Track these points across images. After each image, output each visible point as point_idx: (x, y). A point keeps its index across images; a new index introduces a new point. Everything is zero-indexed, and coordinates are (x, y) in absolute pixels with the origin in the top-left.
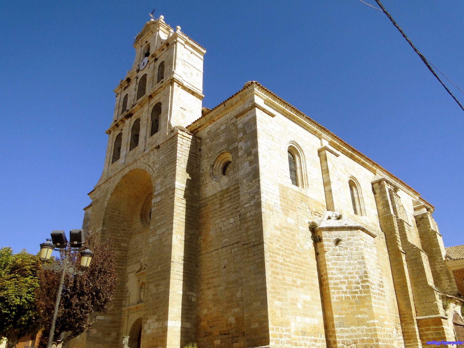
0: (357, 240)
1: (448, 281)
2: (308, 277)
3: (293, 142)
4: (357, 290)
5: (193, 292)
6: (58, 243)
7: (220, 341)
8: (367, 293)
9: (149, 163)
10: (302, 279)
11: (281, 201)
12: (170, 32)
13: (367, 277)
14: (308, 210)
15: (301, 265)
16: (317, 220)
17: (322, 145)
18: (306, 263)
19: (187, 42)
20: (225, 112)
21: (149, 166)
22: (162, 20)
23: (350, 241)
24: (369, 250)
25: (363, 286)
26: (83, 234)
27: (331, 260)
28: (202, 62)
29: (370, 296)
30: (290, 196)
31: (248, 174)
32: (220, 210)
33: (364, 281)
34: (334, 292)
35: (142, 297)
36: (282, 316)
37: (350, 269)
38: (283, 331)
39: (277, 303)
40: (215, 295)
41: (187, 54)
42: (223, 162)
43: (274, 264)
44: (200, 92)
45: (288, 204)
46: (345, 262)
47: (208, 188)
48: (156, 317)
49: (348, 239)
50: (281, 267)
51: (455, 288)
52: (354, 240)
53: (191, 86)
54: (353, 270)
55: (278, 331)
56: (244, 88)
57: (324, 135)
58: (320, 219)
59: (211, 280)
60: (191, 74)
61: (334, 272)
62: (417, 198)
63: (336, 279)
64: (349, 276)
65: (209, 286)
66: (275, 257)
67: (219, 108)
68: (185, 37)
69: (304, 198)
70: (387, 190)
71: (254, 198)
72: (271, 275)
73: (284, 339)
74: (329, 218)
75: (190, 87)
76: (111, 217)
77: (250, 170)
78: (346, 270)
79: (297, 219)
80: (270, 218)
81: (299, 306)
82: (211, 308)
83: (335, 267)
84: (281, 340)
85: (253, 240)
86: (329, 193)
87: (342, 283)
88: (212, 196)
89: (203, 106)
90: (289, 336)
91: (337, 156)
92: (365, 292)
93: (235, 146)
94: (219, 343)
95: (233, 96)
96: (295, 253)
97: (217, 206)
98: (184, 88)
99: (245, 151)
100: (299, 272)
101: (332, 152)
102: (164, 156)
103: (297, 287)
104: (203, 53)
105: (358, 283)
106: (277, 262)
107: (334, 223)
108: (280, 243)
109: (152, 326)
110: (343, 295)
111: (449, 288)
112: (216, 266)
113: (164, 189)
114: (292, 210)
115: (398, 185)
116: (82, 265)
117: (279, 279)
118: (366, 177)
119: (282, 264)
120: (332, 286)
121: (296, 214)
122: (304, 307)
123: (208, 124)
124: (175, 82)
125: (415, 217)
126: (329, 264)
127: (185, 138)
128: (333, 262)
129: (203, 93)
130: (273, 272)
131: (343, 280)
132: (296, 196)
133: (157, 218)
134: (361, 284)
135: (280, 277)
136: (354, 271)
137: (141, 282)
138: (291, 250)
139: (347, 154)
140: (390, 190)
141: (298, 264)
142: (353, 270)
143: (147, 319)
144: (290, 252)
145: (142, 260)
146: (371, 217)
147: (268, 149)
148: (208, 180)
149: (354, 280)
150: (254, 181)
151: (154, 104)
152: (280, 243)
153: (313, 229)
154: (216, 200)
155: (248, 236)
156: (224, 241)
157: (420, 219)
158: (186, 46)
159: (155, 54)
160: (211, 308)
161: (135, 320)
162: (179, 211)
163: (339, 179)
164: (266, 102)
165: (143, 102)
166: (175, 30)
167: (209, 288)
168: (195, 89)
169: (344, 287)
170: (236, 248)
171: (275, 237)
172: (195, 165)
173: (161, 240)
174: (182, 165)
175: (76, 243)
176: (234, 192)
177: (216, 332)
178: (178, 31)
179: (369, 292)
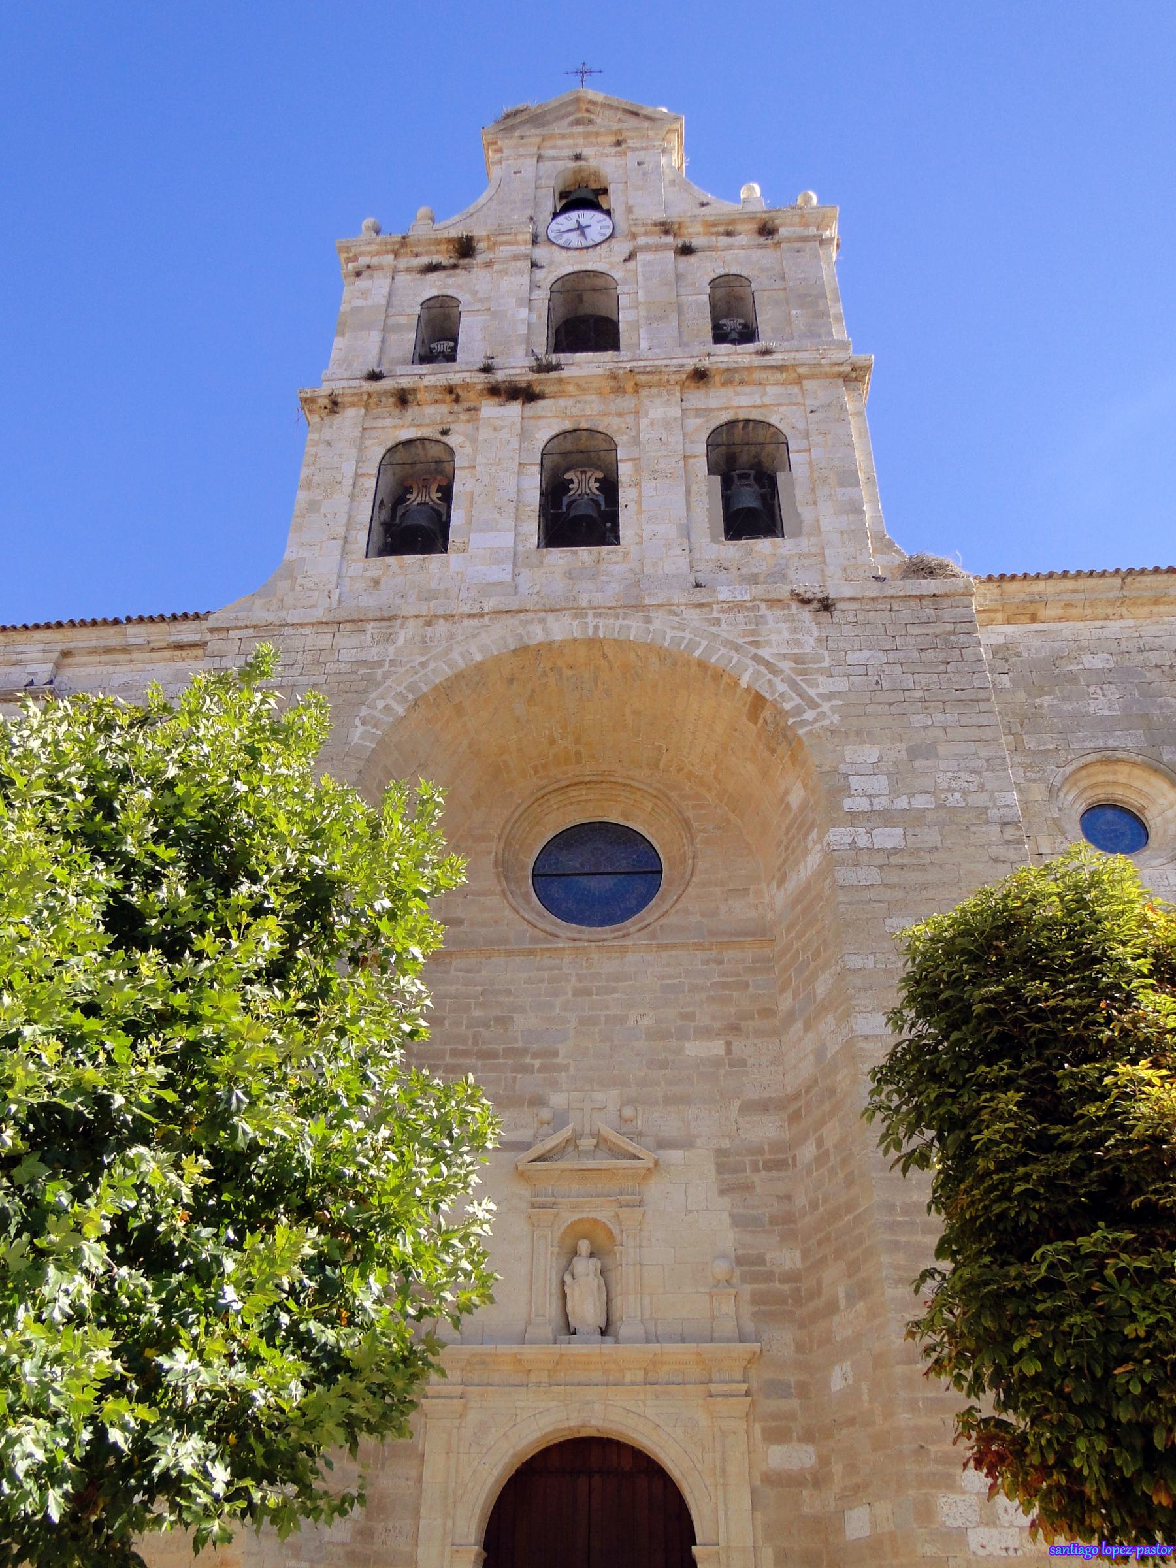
20: (1109, 611)
42: (1110, 790)
151: (725, 417)
159: (680, 225)
165: (643, 378)
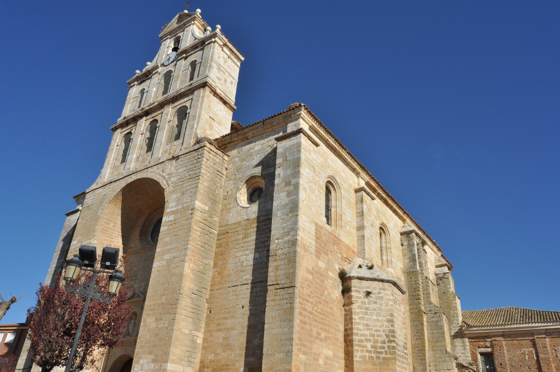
0: (387, 295)
1: (462, 348)
2: (332, 330)
3: (331, 177)
4: (383, 350)
8: (392, 355)
9: (164, 174)
10: (326, 332)
11: (316, 241)
13: (394, 337)
14: (339, 255)
15: (327, 316)
16: (346, 267)
17: (359, 184)
18: (332, 314)
21: (163, 177)
22: (198, 14)
23: (380, 295)
24: (397, 307)
25: (389, 347)
26: (121, 254)
27: (358, 313)
28: (238, 70)
29: (395, 359)
30: (324, 237)
31: (285, 206)
33: (390, 341)
34: (358, 350)
37: (377, 326)
39: (302, 357)
40: (226, 339)
41: (224, 58)
42: (252, 186)
43: (303, 312)
46: (373, 317)
47: (231, 214)
48: (152, 357)
49: (379, 293)
50: (309, 317)
51: (469, 357)
52: (385, 295)
53: (223, 95)
54: (380, 327)
56: (290, 110)
57: (363, 174)
58: (349, 266)
61: (361, 327)
62: (440, 254)
63: (361, 335)
64: (376, 333)
65: (219, 327)
68: (225, 39)
69: (337, 241)
70: (415, 243)
71: (289, 234)
74: (360, 267)
75: (223, 95)
78: (373, 326)
80: (304, 259)
81: (321, 361)
82: (219, 354)
83: (362, 322)
85: (282, 282)
86: (361, 238)
87: (367, 340)
88: (235, 224)
89: (233, 119)
91: (373, 199)
92: (390, 354)
95: (275, 116)
96: (322, 302)
97: (241, 237)
98: (215, 94)
100: (324, 324)
101: (368, 194)
103: (321, 340)
104: (240, 60)
105: (384, 343)
106: (305, 310)
107: (364, 272)
108: (311, 289)
110: (367, 354)
111: (462, 355)
112: (231, 305)
113: (180, 207)
114: (325, 253)
115: (426, 239)
116: (110, 291)
117: (306, 330)
118: (396, 224)
119: (311, 313)
120: (357, 343)
121: (327, 257)
122: (325, 363)
123: (240, 141)
125: (436, 275)
126: (356, 318)
127: (212, 152)
128: (360, 316)
129: (235, 104)
130: (301, 321)
131: (368, 338)
132: (329, 237)
134: (387, 344)
135: (307, 327)
136: (381, 329)
138: (319, 298)
139: (381, 198)
140: (418, 244)
141: (324, 315)
142: (380, 327)
143: (140, 358)
145: (135, 286)
146: (396, 269)
148: (232, 205)
149: (380, 339)
150: (290, 215)
153: (343, 277)
154: (239, 229)
156: (245, 277)
157: (441, 279)
158: (225, 49)
160: (219, 354)
163: (372, 225)
166: (214, 29)
167: (219, 330)
168: (227, 98)
169: (369, 345)
172: (219, 185)
173: (169, 266)
174: (205, 183)
175: (108, 263)
176: (263, 224)
178: (218, 31)
179: (394, 353)
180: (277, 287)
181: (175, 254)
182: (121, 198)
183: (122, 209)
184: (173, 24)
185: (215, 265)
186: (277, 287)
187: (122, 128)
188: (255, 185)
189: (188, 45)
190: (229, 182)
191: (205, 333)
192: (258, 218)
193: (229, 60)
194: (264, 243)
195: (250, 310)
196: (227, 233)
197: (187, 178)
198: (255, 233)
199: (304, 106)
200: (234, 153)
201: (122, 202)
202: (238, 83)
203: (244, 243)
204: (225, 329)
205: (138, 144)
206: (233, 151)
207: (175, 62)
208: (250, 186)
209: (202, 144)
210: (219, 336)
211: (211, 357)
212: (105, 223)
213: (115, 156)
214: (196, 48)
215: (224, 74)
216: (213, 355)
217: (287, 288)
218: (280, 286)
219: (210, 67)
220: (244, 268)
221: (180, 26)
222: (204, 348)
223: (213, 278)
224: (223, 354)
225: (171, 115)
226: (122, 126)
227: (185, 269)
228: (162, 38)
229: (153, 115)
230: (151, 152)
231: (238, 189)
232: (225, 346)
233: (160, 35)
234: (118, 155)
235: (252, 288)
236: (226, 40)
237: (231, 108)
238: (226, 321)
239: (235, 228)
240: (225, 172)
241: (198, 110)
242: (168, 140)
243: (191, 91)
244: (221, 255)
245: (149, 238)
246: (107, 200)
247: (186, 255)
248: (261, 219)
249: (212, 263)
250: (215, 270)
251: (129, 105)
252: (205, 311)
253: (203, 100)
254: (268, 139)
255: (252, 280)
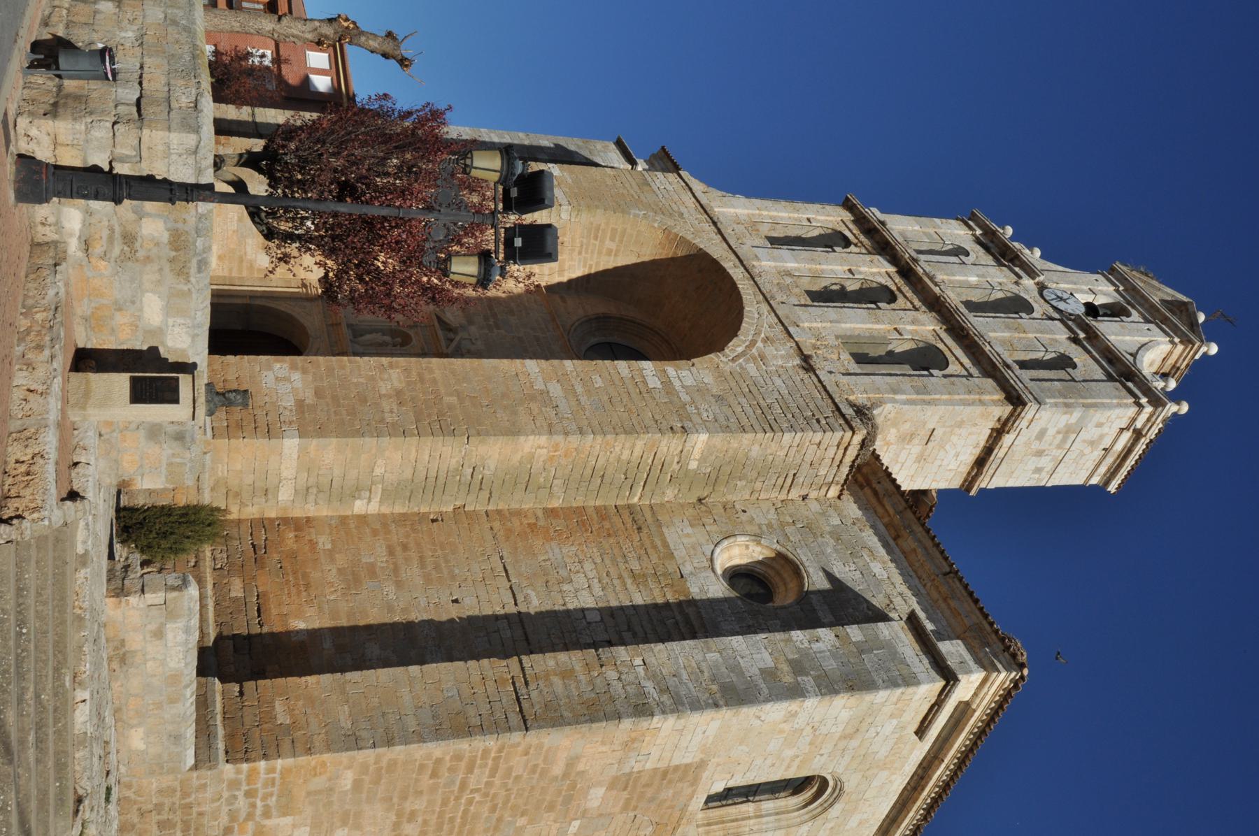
3: (839, 789)
5: (381, 502)
6: (519, 192)
7: (241, 595)
9: (760, 344)
12: (1165, 376)
19: (1138, 434)
21: (753, 343)
22: (1204, 349)
31: (736, 668)
32: (625, 575)
35: (368, 337)
36: (309, 794)
38: (265, 798)
40: (372, 571)
43: (463, 764)
44: (985, 482)
45: (647, 785)
47: (689, 530)
48: (310, 398)
50: (453, 782)
53: (1001, 455)
55: (265, 785)
56: (1002, 640)
59: (413, 554)
60: (1040, 453)
65: (399, 548)
66: (484, 766)
67: (939, 556)
68: (1155, 430)
71: (662, 691)
72: (429, 756)
73: (242, 803)
75: (999, 453)
76: (598, 229)
77: (747, 674)
79: (601, 815)
80: (603, 743)
82: (333, 560)
84: (240, 794)
85: (534, 694)
90: (250, 816)
93: (820, 614)
94: (233, 594)
95: (976, 601)
96: (496, 815)
97: (635, 566)
98: (997, 434)
99: (805, 654)
102: (785, 392)
104: (1107, 482)
106: (470, 769)
108: (525, 776)
109: (284, 388)
112: (457, 571)
113: (685, 397)
114: (628, 801)
117: (417, 780)
121: (617, 809)
123: (886, 520)
124: (1015, 410)
127: (841, 451)
129: (983, 491)
130: (439, 761)
132: (672, 807)
133: (599, 382)
135: (426, 781)
137: (411, 333)
141: (463, 824)
143: (304, 371)
144: (500, 801)
145: (473, 329)
147: (816, 725)
148: (714, 528)
150: (715, 687)
152: (525, 776)
155: (547, 676)
156: (532, 594)
161: (302, 320)
162: (617, 449)
164: (964, 710)
166: (1175, 397)
167: (391, 552)
170: (509, 635)
171: (545, 760)
172: (758, 485)
173: (532, 398)
174: (756, 448)
175: (518, 242)
176: (679, 618)
177: (266, 582)
178: (1172, 408)
180: (520, 683)
181: (563, 405)
182: (680, 253)
183: (653, 262)
184: (1160, 293)
185: (551, 513)
186: (520, 683)
187: (854, 222)
188: (777, 579)
189: (1112, 338)
190: (773, 510)
191: (382, 518)
192: (692, 603)
193: (1098, 453)
194: (629, 629)
195: (452, 621)
196: (639, 529)
197: (761, 402)
198: (649, 601)
199: (1022, 677)
200: (852, 509)
201: (672, 259)
202: (1043, 487)
203: (620, 577)
204: (395, 564)
205: (824, 267)
206: (855, 506)
207: (1057, 316)
208: (773, 568)
209: (856, 423)
210: (377, 554)
211: (324, 542)
212: (614, 231)
213: (782, 218)
214: (1110, 362)
215: (1059, 447)
216: (329, 546)
217: (521, 711)
218: (522, 690)
219: (1067, 405)
220: (556, 588)
221: (1158, 310)
222: (343, 520)
223: (518, 513)
224: (334, 572)
225: (911, 332)
226: (862, 222)
227: (531, 437)
228: (1113, 271)
229: (906, 289)
230: (809, 302)
231: (757, 537)
232: (353, 573)
233: (1118, 266)
234: (786, 226)
235: (506, 617)
236: (1152, 434)
237: (970, 481)
238: (415, 563)
239: (655, 547)
240: (795, 494)
241: (945, 397)
242: (850, 337)
243: (989, 368)
244: (578, 522)
245: (593, 340)
246: (670, 223)
247: (566, 434)
248: (690, 611)
249: (556, 503)
250: (540, 514)
251: (917, 228)
252: (435, 508)
253: (973, 403)
254: (908, 593)
255: (528, 614)
